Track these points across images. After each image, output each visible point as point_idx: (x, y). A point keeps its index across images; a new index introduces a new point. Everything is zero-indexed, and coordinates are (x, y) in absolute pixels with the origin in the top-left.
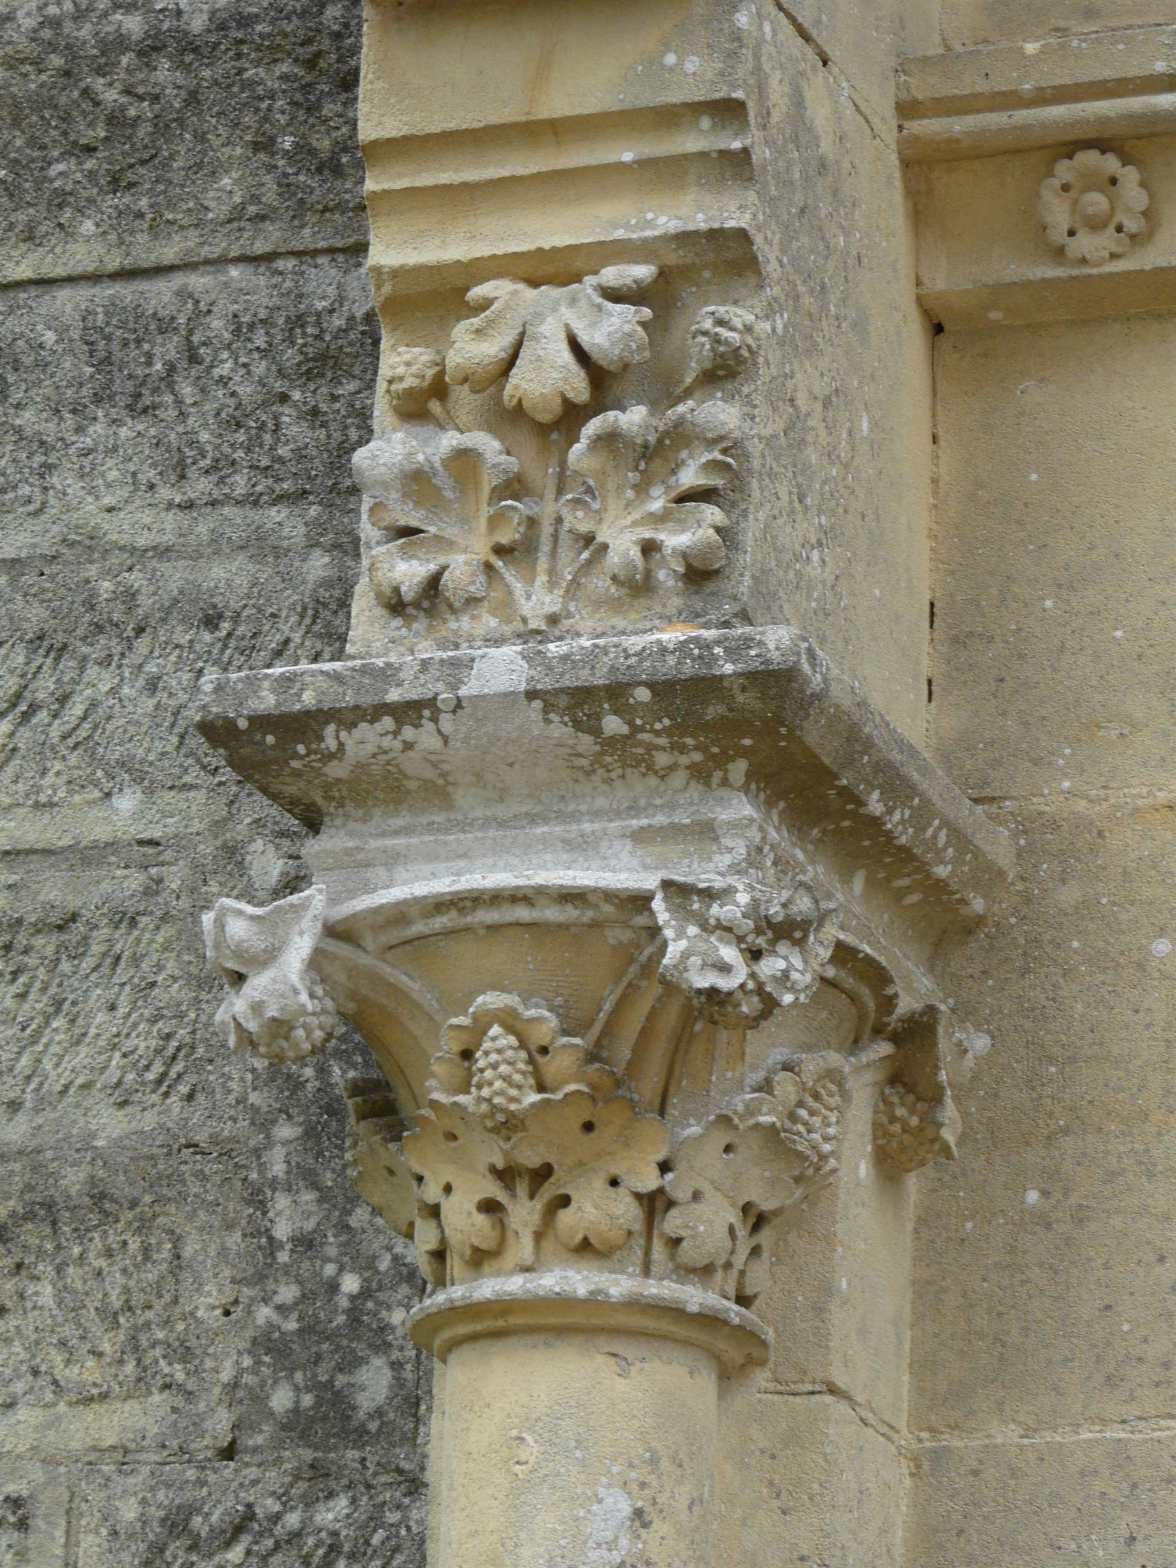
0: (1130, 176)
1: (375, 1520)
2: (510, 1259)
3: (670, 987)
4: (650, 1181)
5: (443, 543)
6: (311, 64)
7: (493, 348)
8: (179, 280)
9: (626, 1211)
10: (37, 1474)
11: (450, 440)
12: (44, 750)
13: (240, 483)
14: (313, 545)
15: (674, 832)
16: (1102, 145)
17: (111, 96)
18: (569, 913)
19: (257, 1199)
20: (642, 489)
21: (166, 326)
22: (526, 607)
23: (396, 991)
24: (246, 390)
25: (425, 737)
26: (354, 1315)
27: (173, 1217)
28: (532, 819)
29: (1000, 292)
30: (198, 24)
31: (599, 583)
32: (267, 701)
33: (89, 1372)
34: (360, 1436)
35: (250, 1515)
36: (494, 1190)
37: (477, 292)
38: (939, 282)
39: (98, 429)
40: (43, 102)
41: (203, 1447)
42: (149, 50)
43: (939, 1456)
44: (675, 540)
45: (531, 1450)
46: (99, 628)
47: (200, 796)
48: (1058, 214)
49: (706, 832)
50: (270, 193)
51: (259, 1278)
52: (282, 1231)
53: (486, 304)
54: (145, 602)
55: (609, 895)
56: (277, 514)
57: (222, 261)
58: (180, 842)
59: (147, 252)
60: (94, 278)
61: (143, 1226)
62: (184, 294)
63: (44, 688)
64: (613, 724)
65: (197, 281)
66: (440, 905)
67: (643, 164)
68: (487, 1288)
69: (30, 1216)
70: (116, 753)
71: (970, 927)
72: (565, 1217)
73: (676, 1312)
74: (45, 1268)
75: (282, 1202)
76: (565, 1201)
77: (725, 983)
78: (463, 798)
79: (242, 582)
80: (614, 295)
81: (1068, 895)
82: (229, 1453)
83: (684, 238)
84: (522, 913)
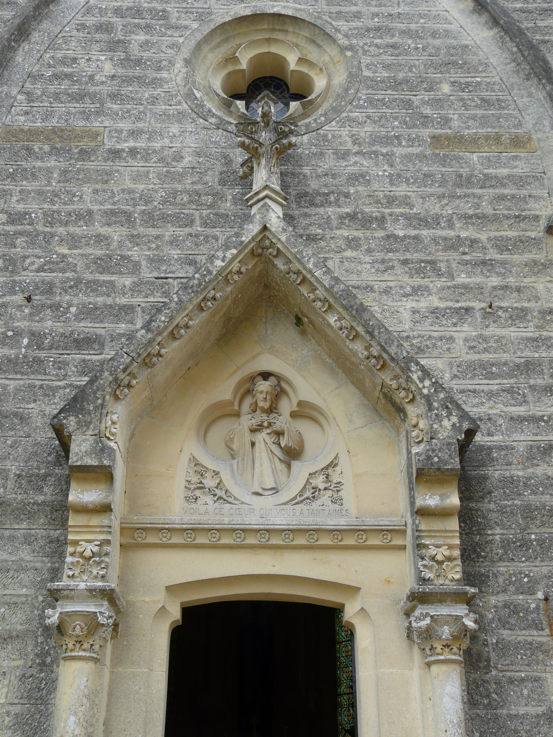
0: (144, 533)
1: (48, 676)
2: (76, 650)
3: (99, 623)
4: (92, 643)
5: (74, 570)
6: (52, 508)
7: (82, 550)
8: (35, 530)
9: (89, 646)
10: (7, 669)
11: (77, 559)
12: (15, 583)
13: (41, 554)
14: (49, 562)
15: (99, 605)
16: (142, 529)
17: (29, 509)
18: (87, 613)
19: (36, 637)
20: (97, 566)
21: (33, 536)
22: (84, 578)
23: (66, 620)
24: (42, 544)
25: (73, 593)
26: (47, 652)
27: (26, 639)
28: (83, 602)
29: (129, 543)
30: (40, 502)
31: (92, 576)
32: (55, 587)
33: (14, 657)
34: (46, 666)
35: (33, 675)
36: (75, 643)
37: (80, 543)
38: (122, 541)
39: (24, 546)
40: (20, 508)
41: (28, 666)
42: (34, 504)
43: (113, 671)
44: (101, 573)
45: (76, 673)
46: (23, 569)
47: (33, 590)
48: (136, 536)
49: (102, 605)
50: (47, 522)
51: (36, 647)
52: (39, 641)
53: (81, 545)
54: (28, 567)
55: (92, 612)
56: (45, 558)
57: (40, 529)
58: (31, 595)
59: (31, 527)
60: (25, 529)
61: (23, 640)
62: (36, 532)
63: (16, 576)
64: (94, 593)
65: (37, 531)
66: (73, 612)
67: (100, 531)
68: (73, 654)
69: (9, 638)
70: (24, 584)
71: (120, 612)
72: (83, 647)
73: (93, 657)
74: (10, 644)
75: (39, 638)
76: (82, 645)
77: (105, 623)
78: (75, 599)
79: (40, 566)
80: (96, 545)
81: (131, 609)
82: (30, 667)
83: (104, 540)
84: (82, 613)
